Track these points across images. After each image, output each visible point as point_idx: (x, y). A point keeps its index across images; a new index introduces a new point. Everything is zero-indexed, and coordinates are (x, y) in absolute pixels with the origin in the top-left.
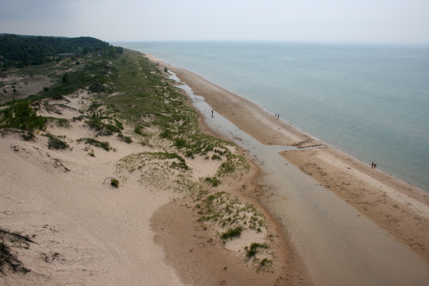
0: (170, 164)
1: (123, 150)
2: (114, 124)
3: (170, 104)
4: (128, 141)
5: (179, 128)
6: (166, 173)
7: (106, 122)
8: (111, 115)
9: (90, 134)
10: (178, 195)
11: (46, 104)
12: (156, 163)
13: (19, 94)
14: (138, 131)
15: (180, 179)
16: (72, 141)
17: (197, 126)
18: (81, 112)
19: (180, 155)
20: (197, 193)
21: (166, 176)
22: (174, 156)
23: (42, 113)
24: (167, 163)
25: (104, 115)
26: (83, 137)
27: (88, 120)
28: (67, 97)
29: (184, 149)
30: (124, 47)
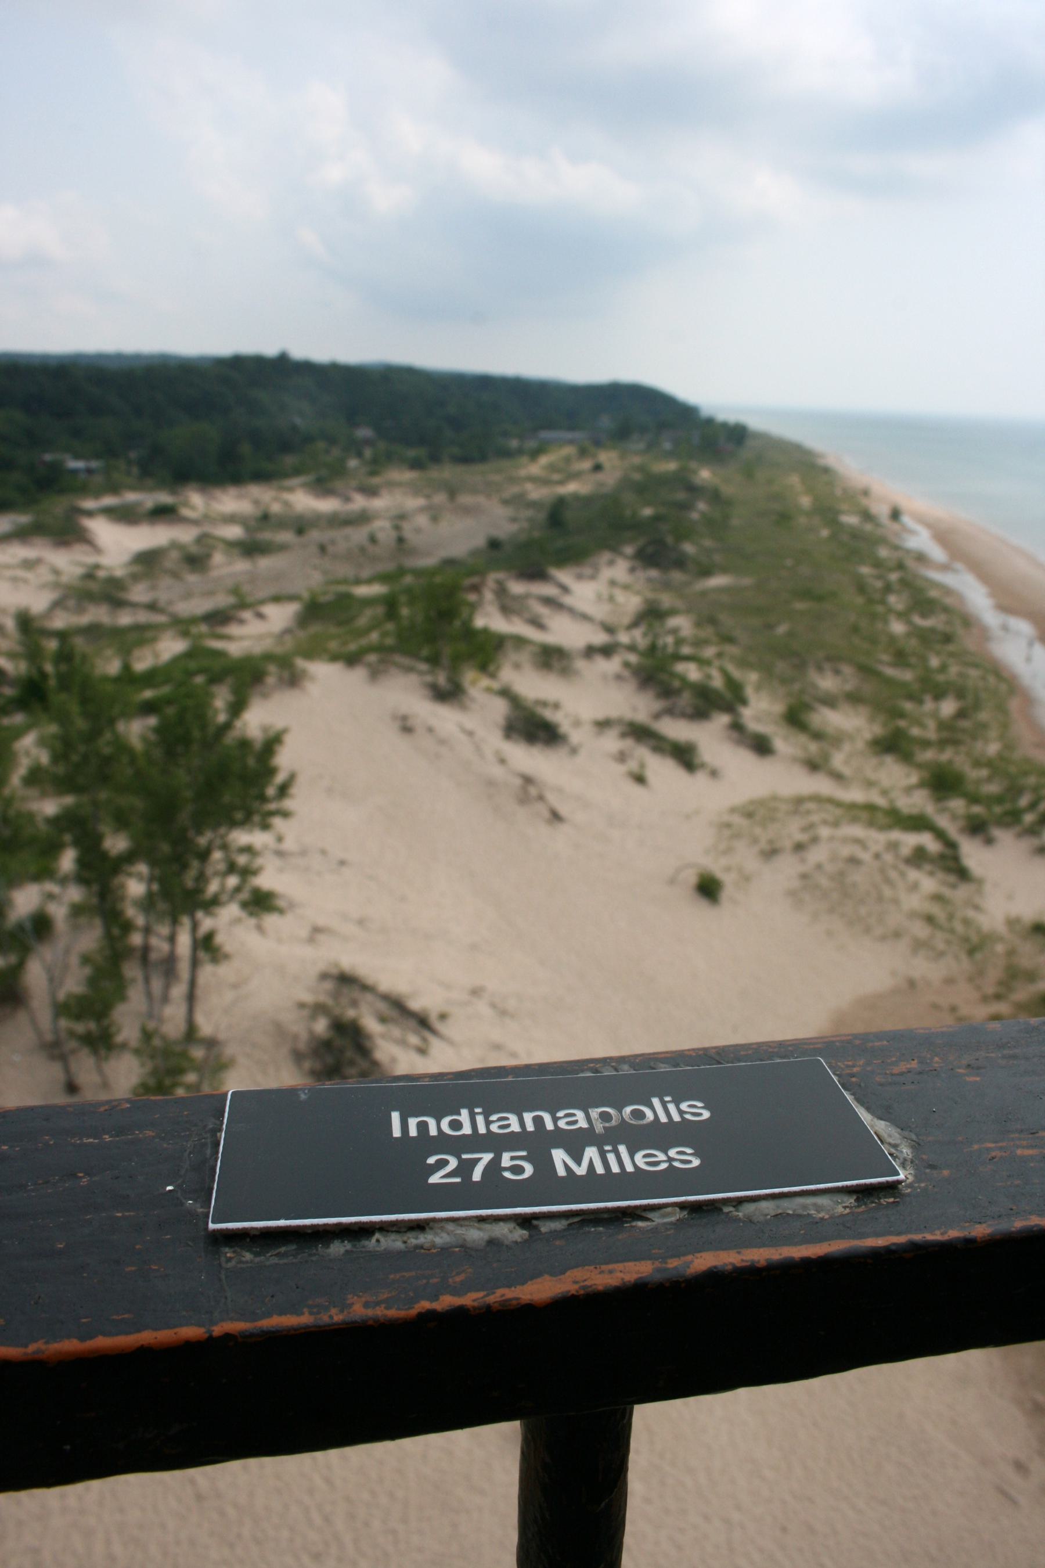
0: (906, 851)
1: (742, 778)
2: (717, 682)
3: (909, 635)
4: (761, 747)
5: (943, 725)
6: (888, 881)
7: (692, 672)
8: (709, 652)
9: (639, 706)
10: (923, 968)
11: (501, 591)
12: (858, 841)
13: (413, 552)
14: (795, 718)
15: (936, 910)
16: (577, 723)
17: (1005, 726)
18: (609, 629)
19: (943, 822)
20: (994, 974)
21: (887, 892)
22: (918, 823)
23: (489, 619)
24: (893, 846)
25: (686, 650)
26: (614, 713)
27: (633, 658)
28: (564, 576)
29: (957, 804)
30: (755, 423)
